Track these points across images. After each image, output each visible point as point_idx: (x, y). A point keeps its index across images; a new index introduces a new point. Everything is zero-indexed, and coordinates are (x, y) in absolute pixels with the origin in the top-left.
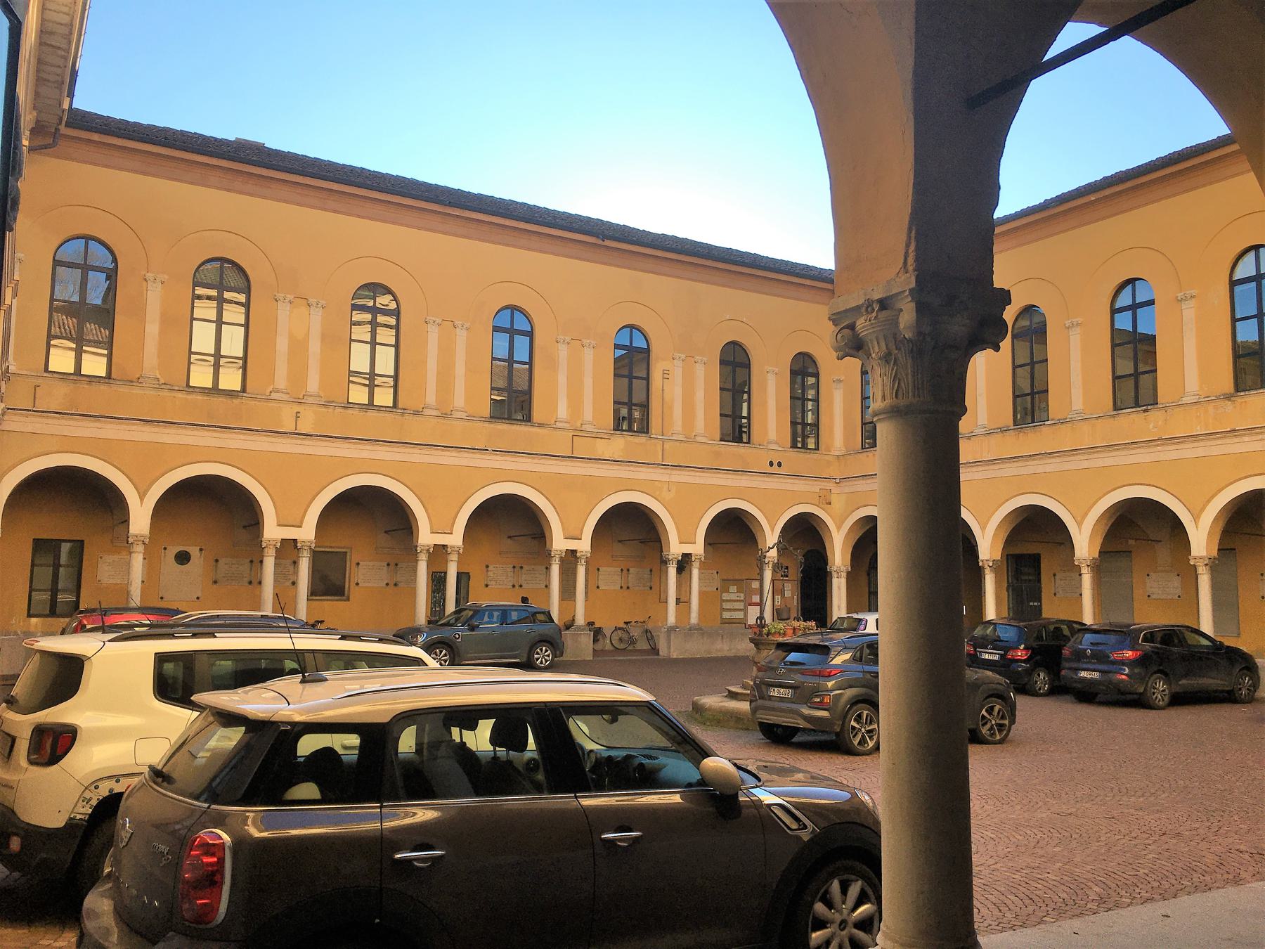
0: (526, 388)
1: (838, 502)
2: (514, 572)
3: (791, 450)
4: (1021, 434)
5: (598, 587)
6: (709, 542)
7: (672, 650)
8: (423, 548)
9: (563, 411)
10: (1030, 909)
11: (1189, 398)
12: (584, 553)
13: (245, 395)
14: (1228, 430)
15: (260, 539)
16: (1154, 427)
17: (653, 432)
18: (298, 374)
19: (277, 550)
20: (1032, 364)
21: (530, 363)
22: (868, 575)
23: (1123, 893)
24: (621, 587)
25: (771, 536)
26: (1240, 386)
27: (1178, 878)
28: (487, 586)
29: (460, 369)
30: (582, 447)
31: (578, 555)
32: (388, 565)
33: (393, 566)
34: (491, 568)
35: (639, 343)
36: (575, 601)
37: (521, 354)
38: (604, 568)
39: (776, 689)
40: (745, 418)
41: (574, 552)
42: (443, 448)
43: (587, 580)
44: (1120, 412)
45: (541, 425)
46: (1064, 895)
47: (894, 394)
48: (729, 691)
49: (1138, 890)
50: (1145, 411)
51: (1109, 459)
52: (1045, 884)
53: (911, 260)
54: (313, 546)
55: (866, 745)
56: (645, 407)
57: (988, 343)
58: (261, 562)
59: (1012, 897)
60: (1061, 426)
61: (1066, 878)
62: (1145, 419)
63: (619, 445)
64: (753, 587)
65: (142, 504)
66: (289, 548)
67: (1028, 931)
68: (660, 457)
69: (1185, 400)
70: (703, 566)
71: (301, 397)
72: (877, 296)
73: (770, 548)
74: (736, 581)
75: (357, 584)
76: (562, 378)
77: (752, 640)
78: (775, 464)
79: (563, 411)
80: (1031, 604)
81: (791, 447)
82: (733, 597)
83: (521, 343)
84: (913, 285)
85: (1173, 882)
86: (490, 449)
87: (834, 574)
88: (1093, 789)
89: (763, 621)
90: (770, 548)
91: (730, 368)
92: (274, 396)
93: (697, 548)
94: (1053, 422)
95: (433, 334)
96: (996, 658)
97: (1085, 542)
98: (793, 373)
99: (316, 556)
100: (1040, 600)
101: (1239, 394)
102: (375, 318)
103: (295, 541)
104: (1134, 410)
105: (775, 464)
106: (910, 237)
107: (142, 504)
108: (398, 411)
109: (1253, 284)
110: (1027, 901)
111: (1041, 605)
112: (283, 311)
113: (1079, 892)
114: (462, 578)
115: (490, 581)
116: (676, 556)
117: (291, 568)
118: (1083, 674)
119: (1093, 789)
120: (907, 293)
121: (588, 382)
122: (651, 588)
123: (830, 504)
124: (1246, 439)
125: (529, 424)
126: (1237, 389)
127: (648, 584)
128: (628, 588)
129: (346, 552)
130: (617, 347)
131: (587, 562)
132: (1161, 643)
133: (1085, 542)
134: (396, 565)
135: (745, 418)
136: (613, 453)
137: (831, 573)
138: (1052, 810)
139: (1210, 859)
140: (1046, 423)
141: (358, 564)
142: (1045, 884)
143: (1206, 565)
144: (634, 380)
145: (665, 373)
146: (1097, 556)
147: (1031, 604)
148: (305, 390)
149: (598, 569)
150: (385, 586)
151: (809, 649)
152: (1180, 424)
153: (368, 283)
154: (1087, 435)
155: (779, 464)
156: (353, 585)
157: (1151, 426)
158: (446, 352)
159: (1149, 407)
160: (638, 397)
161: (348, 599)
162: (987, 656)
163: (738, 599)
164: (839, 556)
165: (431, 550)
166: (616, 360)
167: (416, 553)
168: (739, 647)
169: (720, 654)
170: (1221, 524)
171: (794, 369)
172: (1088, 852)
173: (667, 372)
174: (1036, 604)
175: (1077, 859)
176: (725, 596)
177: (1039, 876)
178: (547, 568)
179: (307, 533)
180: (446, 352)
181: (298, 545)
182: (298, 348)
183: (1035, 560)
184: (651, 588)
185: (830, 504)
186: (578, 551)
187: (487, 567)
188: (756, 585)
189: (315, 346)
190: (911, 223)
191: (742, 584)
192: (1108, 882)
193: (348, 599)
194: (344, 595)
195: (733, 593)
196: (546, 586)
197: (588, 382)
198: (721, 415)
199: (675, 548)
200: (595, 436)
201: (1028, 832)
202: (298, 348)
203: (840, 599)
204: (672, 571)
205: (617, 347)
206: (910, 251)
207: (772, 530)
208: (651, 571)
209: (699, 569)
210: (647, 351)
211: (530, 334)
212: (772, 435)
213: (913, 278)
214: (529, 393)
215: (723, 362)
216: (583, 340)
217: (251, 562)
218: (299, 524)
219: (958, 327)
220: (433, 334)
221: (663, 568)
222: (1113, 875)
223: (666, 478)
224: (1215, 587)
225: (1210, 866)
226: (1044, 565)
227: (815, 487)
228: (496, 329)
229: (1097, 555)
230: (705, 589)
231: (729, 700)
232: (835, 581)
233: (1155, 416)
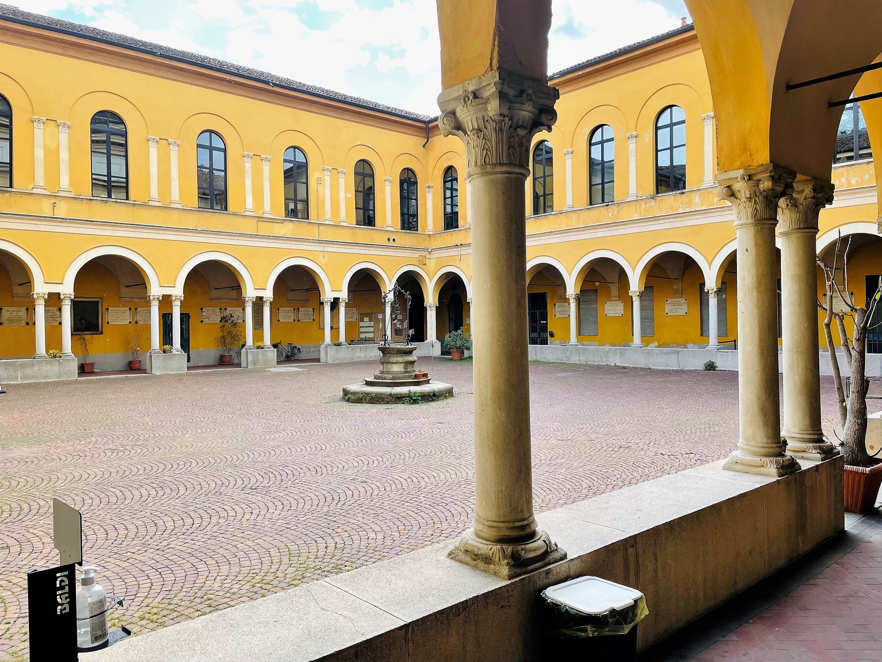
0: (223, 188)
1: (431, 264)
2: (221, 312)
3: (401, 231)
4: (538, 220)
5: (279, 320)
6: (350, 290)
7: (328, 359)
8: (154, 297)
9: (249, 203)
10: (550, 496)
11: (631, 198)
12: (269, 299)
13: (13, 190)
14: (652, 216)
15: (32, 293)
16: (612, 216)
17: (312, 219)
18: (53, 174)
19: (46, 301)
20: (544, 177)
21: (225, 171)
23: (601, 482)
24: (294, 320)
25: (389, 286)
26: (657, 192)
27: (631, 471)
28: (202, 322)
29: (174, 173)
30: (265, 229)
31: (264, 299)
32: (130, 309)
33: (134, 310)
34: (204, 310)
35: (300, 158)
36: (263, 330)
37: (218, 163)
38: (283, 309)
40: (371, 210)
41: (261, 298)
43: (271, 316)
44: (593, 206)
45: (234, 214)
46: (568, 487)
47: (483, 160)
48: (366, 381)
49: (609, 480)
50: (607, 206)
52: (558, 481)
53: (495, 62)
54: (73, 297)
56: (306, 202)
57: (543, 125)
58: (34, 309)
59: (540, 490)
60: (560, 215)
61: (568, 476)
63: (289, 228)
65: (634, 271)
66: (54, 300)
67: (559, 510)
68: (317, 237)
69: (629, 199)
70: (347, 305)
71: (56, 191)
72: (471, 88)
73: (390, 291)
74: (367, 315)
75: (108, 323)
76: (248, 182)
77: (380, 349)
78: (391, 240)
79: (249, 203)
80: (542, 322)
81: (401, 229)
82: (367, 324)
83: (218, 156)
84: (497, 79)
85: (628, 474)
86: (199, 229)
87: (428, 309)
88: (579, 424)
89: (386, 337)
90: (390, 291)
91: (361, 177)
92: (35, 191)
93: (343, 295)
94: (556, 213)
95: (153, 151)
97: (572, 288)
98: (402, 183)
99: (75, 304)
100: (547, 320)
101: (658, 195)
102: (108, 138)
103: (59, 294)
104: (601, 205)
105: (391, 240)
106: (494, 45)
107: (634, 271)
108: (130, 202)
109: (669, 129)
110: (549, 492)
111: (547, 323)
112: (39, 131)
113: (577, 484)
114: (185, 318)
115: (204, 318)
116: (329, 299)
117: (58, 313)
119: (579, 424)
120: (493, 85)
121: (267, 185)
122: (314, 320)
123: (425, 265)
124: (662, 222)
125: (226, 212)
126: (657, 192)
127: (312, 318)
128: (299, 320)
129: (98, 301)
130: (285, 161)
131: (271, 303)
133: (572, 288)
134: (136, 309)
135: (371, 210)
136: (286, 233)
137: (426, 307)
138: (558, 438)
139: (647, 460)
140: (552, 213)
141: (108, 309)
142: (558, 481)
143: (638, 296)
145: (319, 181)
147: (542, 322)
148: (58, 187)
149: (278, 309)
150: (128, 323)
152: (627, 213)
153: (99, 112)
154: (574, 221)
155: (394, 240)
156: (105, 323)
157: (610, 215)
158: (165, 164)
159: (610, 203)
160: (301, 195)
161: (102, 333)
163: (370, 325)
164: (431, 298)
165: (161, 298)
166: (286, 172)
167: (149, 302)
168: (371, 355)
169: (359, 360)
170: (646, 272)
172: (580, 460)
173: (320, 179)
174: (544, 322)
175: (575, 465)
176: (361, 324)
177: (554, 477)
178: (243, 309)
179: (67, 289)
180: (165, 164)
181: (61, 296)
182: (52, 156)
183: (543, 296)
184: (314, 320)
185: (425, 265)
186: (264, 297)
187: (202, 309)
188: (380, 316)
189: (64, 155)
190: (495, 34)
191: (371, 316)
192: (593, 477)
193: (102, 333)
194: (98, 330)
195: (366, 322)
196: (243, 321)
197: (267, 185)
198: (356, 208)
199: (328, 295)
200: (273, 221)
201: (546, 452)
202: (52, 156)
203: (432, 324)
204: (327, 309)
205: (285, 161)
206: (494, 55)
207: (390, 282)
208: (313, 309)
209: (345, 307)
210: (306, 165)
211: (225, 151)
212: (389, 221)
213: (497, 74)
214: (225, 193)
215: (356, 173)
216: (262, 156)
217: (27, 309)
218: (61, 282)
219: (526, 112)
220: (153, 151)
221: (321, 307)
222: (595, 473)
223: (321, 249)
224: (642, 309)
225: (647, 464)
226: (549, 300)
227: (416, 255)
228: (199, 146)
229: (579, 292)
230: (349, 320)
231: (366, 386)
232: (429, 312)
233: (613, 209)
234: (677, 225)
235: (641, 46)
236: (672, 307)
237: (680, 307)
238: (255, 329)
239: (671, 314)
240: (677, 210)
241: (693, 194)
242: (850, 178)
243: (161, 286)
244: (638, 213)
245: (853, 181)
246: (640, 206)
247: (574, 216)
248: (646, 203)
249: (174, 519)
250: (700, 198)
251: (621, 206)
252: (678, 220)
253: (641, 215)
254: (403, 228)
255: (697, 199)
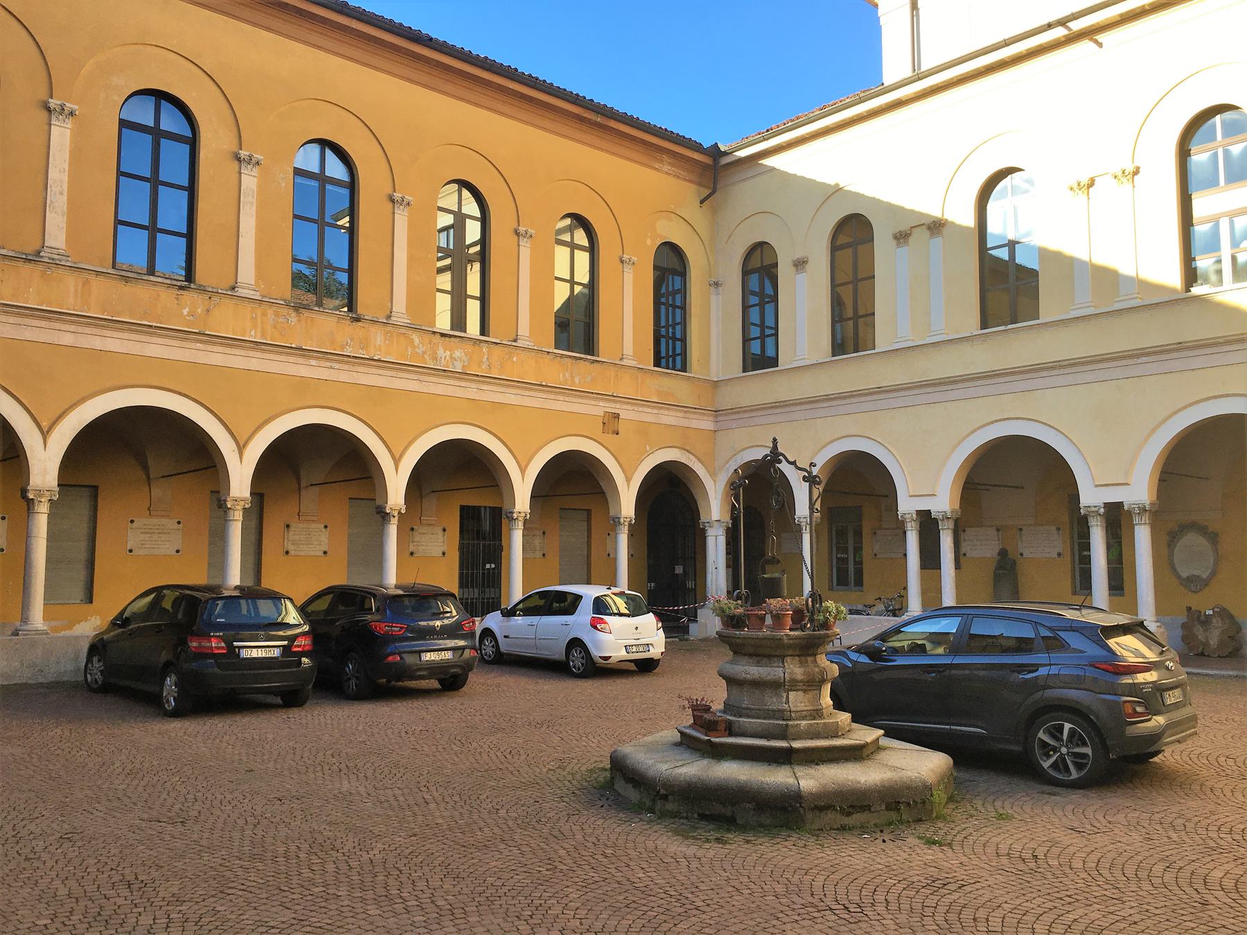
11: (246, 291)
16: (190, 314)
22: (1169, 546)
39: (1171, 693)
42: (76, 269)
51: (114, 342)
55: (1045, 758)
62: (177, 299)
64: (677, 572)
65: (628, 485)
96: (276, 653)
107: (628, 485)
118: (428, 657)
132: (578, 598)
144: (147, 173)
146: (958, 508)
151: (633, 667)
157: (185, 312)
162: (255, 654)
171: (657, 264)
207: (628, 480)
232: (710, 542)
234: (343, 377)
235: (380, 23)
236: (146, 537)
237: (164, 537)
238: (924, 566)
239: (141, 552)
240: (342, 348)
241: (374, 329)
242: (574, 375)
243: (1096, 486)
244: (259, 330)
245: (577, 381)
246: (264, 314)
247: (71, 282)
248: (277, 314)
249: (1160, 880)
250: (385, 340)
251: (216, 299)
252: (346, 367)
253: (263, 336)
254: (657, 363)
255: (379, 339)
